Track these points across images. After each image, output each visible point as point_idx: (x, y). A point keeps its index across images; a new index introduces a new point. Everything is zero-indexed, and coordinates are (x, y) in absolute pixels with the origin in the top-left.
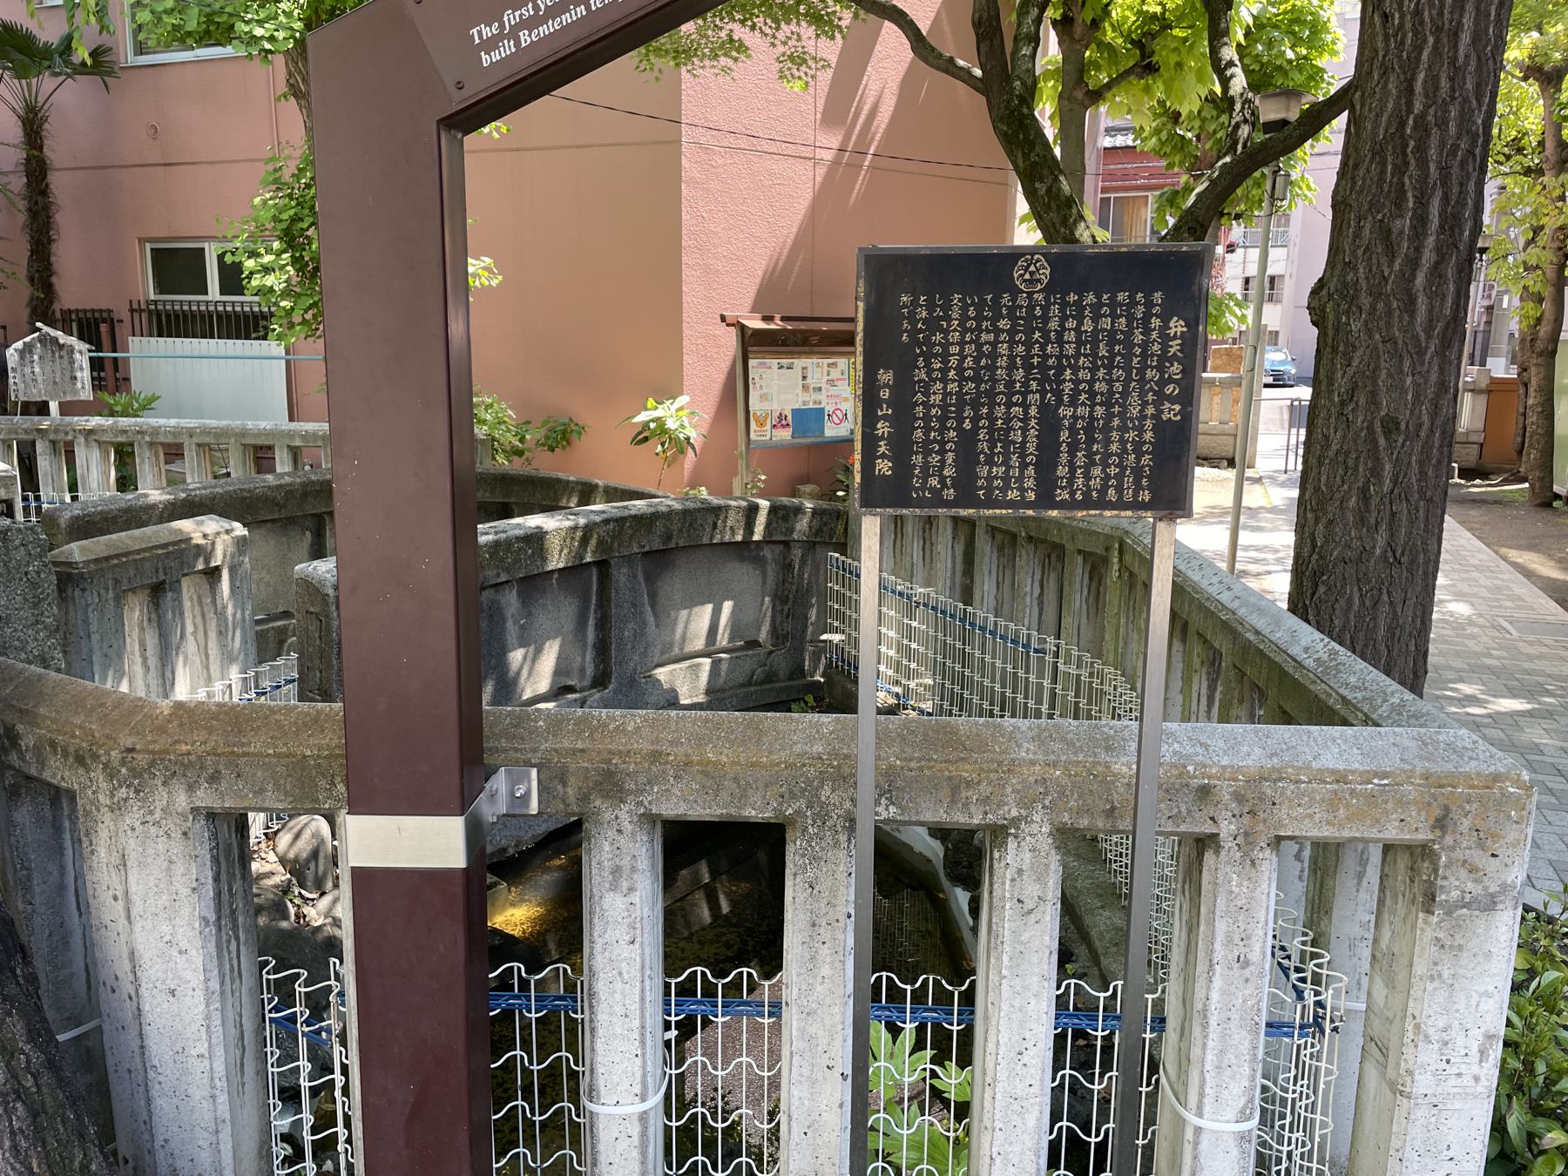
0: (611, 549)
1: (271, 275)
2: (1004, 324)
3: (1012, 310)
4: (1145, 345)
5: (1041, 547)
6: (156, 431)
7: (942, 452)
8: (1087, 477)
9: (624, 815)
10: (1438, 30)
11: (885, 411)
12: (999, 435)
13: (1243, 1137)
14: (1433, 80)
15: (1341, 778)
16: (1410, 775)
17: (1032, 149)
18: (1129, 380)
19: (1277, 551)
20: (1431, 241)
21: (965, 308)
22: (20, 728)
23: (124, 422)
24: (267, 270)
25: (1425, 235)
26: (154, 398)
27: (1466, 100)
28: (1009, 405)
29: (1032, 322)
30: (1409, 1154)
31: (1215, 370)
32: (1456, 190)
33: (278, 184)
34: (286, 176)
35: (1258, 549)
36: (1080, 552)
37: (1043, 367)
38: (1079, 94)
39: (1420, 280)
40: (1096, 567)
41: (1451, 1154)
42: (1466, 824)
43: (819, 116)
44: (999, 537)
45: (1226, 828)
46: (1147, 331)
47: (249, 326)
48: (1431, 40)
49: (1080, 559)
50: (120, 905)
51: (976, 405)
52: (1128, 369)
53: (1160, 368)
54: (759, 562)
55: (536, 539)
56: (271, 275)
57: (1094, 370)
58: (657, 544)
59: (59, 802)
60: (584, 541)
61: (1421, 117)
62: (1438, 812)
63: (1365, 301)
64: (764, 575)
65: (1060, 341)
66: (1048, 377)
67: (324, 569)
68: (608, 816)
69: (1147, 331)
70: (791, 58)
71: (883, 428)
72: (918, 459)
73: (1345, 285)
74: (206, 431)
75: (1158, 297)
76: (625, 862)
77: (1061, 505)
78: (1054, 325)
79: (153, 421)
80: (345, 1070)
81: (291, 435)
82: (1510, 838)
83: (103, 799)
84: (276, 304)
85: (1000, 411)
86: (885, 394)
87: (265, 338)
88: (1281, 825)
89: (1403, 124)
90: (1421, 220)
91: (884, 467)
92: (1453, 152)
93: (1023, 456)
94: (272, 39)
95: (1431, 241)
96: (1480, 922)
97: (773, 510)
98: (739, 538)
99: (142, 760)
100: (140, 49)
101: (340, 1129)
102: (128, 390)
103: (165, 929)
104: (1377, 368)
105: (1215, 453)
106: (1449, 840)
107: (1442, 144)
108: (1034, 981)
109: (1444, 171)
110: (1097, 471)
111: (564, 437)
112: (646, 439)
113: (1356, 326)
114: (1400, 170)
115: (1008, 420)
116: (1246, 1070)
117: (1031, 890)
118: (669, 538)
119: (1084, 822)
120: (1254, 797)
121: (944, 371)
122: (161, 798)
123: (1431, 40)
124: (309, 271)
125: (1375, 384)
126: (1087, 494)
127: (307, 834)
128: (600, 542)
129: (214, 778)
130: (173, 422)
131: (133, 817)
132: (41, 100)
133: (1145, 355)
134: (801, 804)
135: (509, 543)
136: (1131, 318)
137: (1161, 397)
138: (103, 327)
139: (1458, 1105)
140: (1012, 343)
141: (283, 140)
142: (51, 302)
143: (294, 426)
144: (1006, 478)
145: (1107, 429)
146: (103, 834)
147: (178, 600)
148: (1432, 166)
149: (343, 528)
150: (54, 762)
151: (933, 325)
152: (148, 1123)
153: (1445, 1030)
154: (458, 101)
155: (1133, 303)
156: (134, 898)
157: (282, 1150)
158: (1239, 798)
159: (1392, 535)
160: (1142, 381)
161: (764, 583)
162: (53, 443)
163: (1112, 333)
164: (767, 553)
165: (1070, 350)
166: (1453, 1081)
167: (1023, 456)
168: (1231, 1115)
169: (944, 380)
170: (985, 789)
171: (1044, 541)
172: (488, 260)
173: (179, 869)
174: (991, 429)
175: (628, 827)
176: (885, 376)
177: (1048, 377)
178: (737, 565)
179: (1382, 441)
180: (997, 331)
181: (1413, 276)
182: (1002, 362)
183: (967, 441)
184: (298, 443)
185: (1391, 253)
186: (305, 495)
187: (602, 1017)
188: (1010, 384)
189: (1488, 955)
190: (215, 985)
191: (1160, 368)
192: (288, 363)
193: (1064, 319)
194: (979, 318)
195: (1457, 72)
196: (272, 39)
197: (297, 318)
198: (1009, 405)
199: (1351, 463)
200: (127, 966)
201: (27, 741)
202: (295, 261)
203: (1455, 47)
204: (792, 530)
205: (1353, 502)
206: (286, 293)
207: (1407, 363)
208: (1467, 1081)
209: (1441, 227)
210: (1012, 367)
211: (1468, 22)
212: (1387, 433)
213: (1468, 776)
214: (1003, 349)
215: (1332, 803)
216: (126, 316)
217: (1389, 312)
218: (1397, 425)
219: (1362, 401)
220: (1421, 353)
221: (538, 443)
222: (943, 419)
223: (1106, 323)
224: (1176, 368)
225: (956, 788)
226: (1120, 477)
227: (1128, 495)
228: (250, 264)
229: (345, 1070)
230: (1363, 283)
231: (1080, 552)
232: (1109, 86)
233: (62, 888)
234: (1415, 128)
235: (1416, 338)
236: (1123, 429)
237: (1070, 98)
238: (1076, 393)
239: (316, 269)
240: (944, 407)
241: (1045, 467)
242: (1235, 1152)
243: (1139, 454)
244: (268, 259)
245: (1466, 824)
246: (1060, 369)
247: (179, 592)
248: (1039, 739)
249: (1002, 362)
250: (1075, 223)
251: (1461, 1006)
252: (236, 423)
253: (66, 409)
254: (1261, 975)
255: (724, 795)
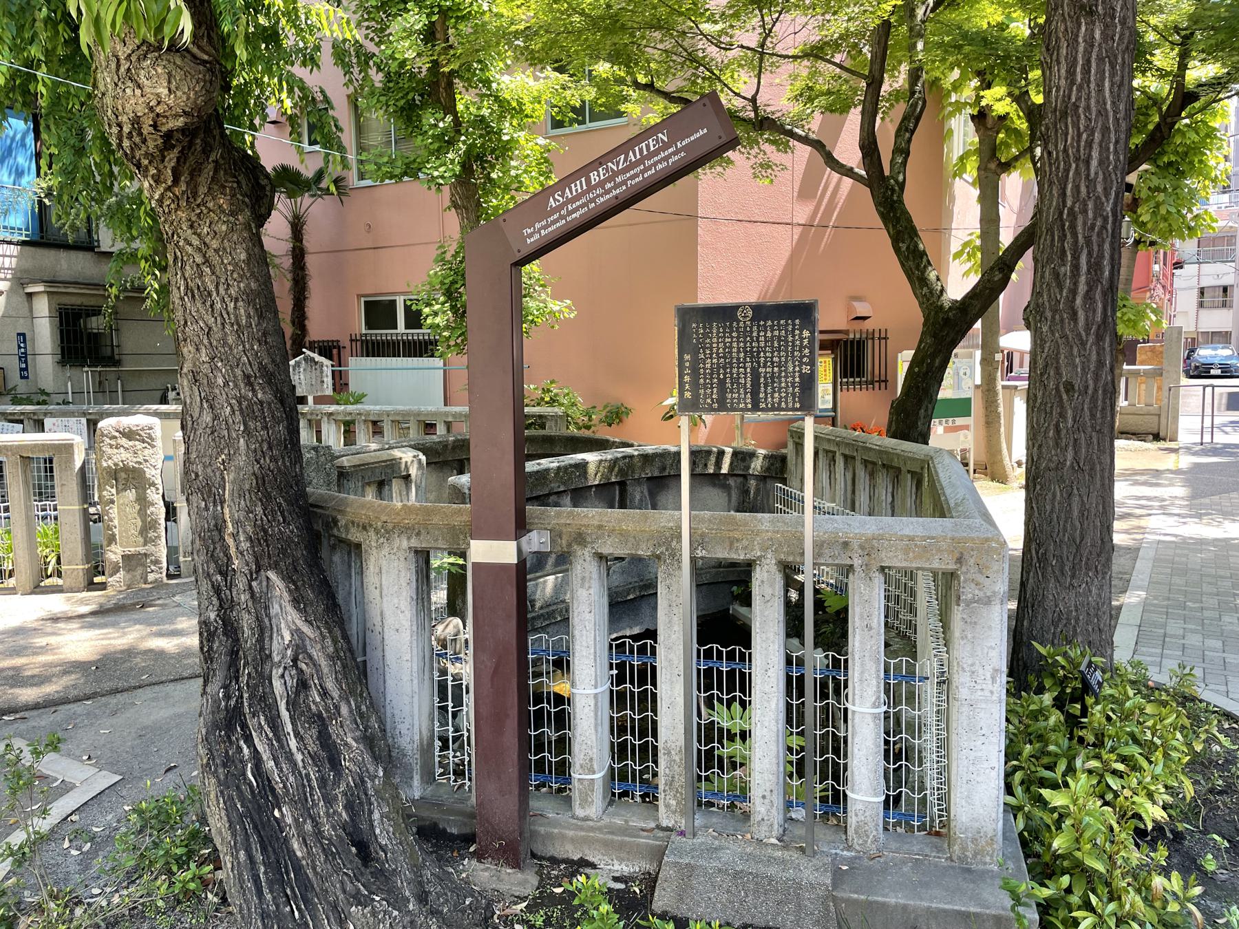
0: (627, 474)
1: (438, 317)
2: (734, 334)
3: (738, 328)
4: (793, 342)
5: (891, 471)
6: (368, 413)
7: (712, 388)
8: (773, 398)
9: (586, 553)
10: (1077, 160)
11: (687, 371)
12: (734, 381)
13: (876, 717)
14: (1077, 188)
15: (911, 539)
16: (945, 538)
17: (898, 222)
18: (787, 356)
19: (1164, 500)
20: (1083, 279)
21: (718, 328)
22: (339, 517)
23: (350, 408)
24: (436, 314)
25: (1079, 275)
26: (364, 396)
27: (1098, 198)
28: (739, 368)
29: (746, 333)
30: (961, 731)
31: (1142, 364)
32: (1096, 248)
33: (441, 260)
34: (448, 257)
35: (1149, 499)
36: (909, 472)
37: (751, 352)
38: (993, 166)
39: (1079, 301)
40: (918, 479)
41: (983, 732)
42: (972, 561)
43: (795, 194)
44: (870, 466)
45: (857, 562)
46: (794, 336)
47: (421, 349)
48: (1074, 166)
49: (909, 476)
50: (378, 591)
51: (725, 368)
52: (787, 352)
53: (800, 351)
54: (726, 488)
55: (583, 466)
56: (438, 317)
57: (772, 352)
58: (656, 474)
59: (356, 549)
60: (611, 469)
61: (1071, 209)
62: (958, 555)
63: (1049, 314)
64: (729, 495)
65: (758, 341)
66: (754, 355)
67: (464, 479)
68: (580, 553)
69: (794, 336)
70: (761, 165)
71: (687, 379)
72: (702, 391)
73: (1038, 305)
74: (398, 413)
75: (797, 321)
76: (587, 575)
77: (762, 410)
78: (755, 334)
79: (367, 407)
80: (468, 731)
81: (446, 414)
82: (995, 568)
83: (373, 544)
84: (440, 335)
85: (735, 370)
86: (687, 364)
87: (432, 356)
88: (882, 560)
89: (1061, 213)
90: (1076, 267)
91: (688, 395)
92: (1092, 227)
93: (745, 389)
94: (442, 177)
95: (1083, 279)
96: (984, 610)
97: (735, 454)
98: (711, 471)
99: (390, 526)
100: (362, 177)
101: (464, 708)
102: (347, 390)
103: (396, 601)
104: (1058, 353)
105: (1142, 429)
106: (964, 569)
107: (1085, 223)
108: (771, 635)
109: (1088, 241)
110: (776, 395)
111: (617, 417)
112: (672, 417)
113: (1045, 329)
114: (1063, 238)
115: (738, 374)
116: (874, 682)
117: (768, 591)
118: (664, 469)
119: (790, 559)
120: (868, 548)
121: (711, 354)
122: (397, 542)
123: (1074, 166)
124: (460, 313)
125: (1058, 362)
126: (773, 405)
127: (451, 626)
128: (621, 470)
129: (418, 534)
130: (378, 408)
131: (385, 551)
132: (302, 211)
133: (793, 346)
134: (663, 549)
135: (566, 468)
136: (786, 331)
137: (801, 363)
138: (335, 351)
139: (984, 706)
140: (738, 342)
141: (447, 234)
142: (304, 336)
143: (448, 409)
144: (739, 399)
145: (779, 377)
146: (372, 559)
147: (390, 490)
148: (1080, 236)
149: (476, 454)
150: (353, 530)
151: (705, 335)
152: (384, 693)
153: (972, 665)
154: (518, 257)
155: (787, 324)
156: (385, 587)
157: (438, 743)
158: (862, 547)
159: (1076, 453)
160: (793, 356)
161: (730, 501)
162: (309, 421)
163: (779, 337)
164: (731, 482)
165: (762, 344)
166: (980, 693)
167: (745, 389)
168: (869, 705)
169: (711, 358)
170: (745, 542)
171: (892, 467)
172: (568, 302)
173: (403, 574)
174: (731, 378)
175: (588, 559)
176: (687, 357)
177: (754, 355)
178: (711, 489)
179: (1065, 397)
180: (732, 337)
181: (1074, 299)
182: (735, 350)
183: (722, 383)
184: (450, 419)
185: (1060, 287)
186: (454, 448)
187: (577, 647)
188: (738, 359)
189: (990, 628)
190: (415, 628)
191: (800, 351)
192: (445, 371)
193: (759, 332)
194: (724, 332)
195: (1091, 183)
196: (442, 177)
197: (452, 343)
198: (739, 368)
199: (1048, 410)
200: (379, 619)
201: (342, 523)
202: (453, 307)
203: (1088, 168)
204: (749, 467)
205: (1051, 434)
206: (447, 327)
207: (1075, 350)
208: (987, 693)
209: (1088, 270)
210: (739, 352)
211: (1095, 154)
212: (1067, 391)
213: (973, 539)
214: (735, 345)
215: (906, 551)
216: (348, 344)
217: (1062, 320)
218: (1073, 386)
219: (1052, 373)
220: (1083, 344)
221: (601, 421)
222: (711, 374)
223: (776, 333)
224: (807, 351)
225: (732, 542)
226: (786, 397)
227: (790, 405)
228: (427, 310)
229: (468, 731)
230: (1047, 304)
231: (909, 472)
232: (1016, 158)
233: (350, 593)
234: (1069, 214)
235: (1079, 335)
236: (786, 377)
237: (986, 169)
238: (766, 362)
239: (464, 312)
240: (712, 369)
241: (755, 393)
242: (872, 725)
243: (794, 388)
244: (437, 307)
245: (972, 561)
246: (759, 353)
247: (390, 486)
248: (772, 522)
249: (735, 350)
250: (925, 267)
251: (979, 653)
252: (415, 408)
253: (318, 400)
254: (878, 634)
255: (630, 544)
